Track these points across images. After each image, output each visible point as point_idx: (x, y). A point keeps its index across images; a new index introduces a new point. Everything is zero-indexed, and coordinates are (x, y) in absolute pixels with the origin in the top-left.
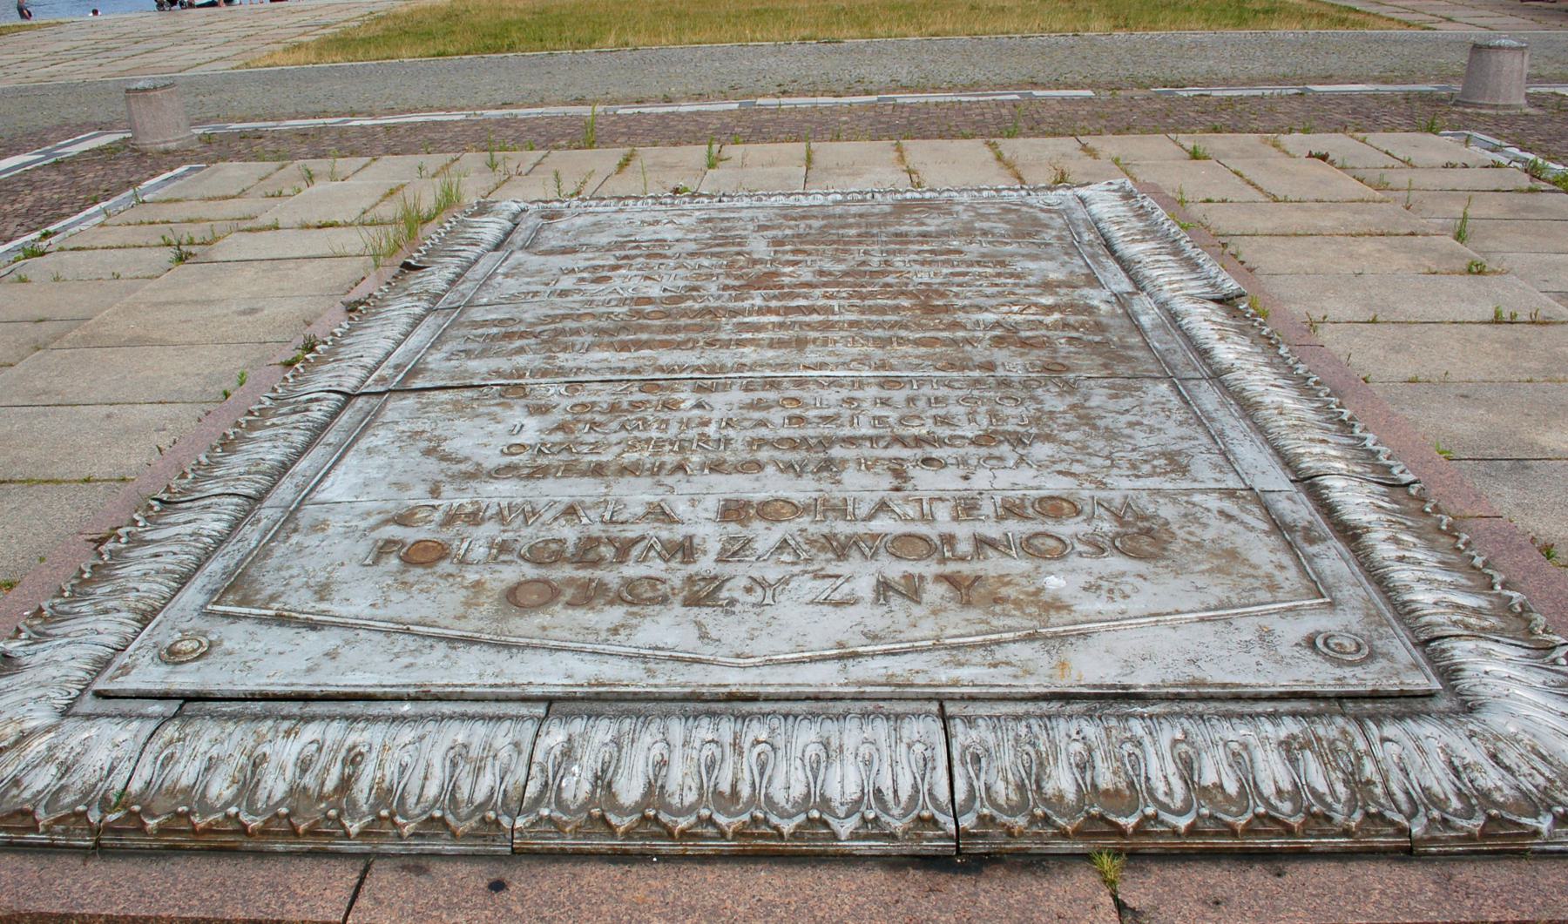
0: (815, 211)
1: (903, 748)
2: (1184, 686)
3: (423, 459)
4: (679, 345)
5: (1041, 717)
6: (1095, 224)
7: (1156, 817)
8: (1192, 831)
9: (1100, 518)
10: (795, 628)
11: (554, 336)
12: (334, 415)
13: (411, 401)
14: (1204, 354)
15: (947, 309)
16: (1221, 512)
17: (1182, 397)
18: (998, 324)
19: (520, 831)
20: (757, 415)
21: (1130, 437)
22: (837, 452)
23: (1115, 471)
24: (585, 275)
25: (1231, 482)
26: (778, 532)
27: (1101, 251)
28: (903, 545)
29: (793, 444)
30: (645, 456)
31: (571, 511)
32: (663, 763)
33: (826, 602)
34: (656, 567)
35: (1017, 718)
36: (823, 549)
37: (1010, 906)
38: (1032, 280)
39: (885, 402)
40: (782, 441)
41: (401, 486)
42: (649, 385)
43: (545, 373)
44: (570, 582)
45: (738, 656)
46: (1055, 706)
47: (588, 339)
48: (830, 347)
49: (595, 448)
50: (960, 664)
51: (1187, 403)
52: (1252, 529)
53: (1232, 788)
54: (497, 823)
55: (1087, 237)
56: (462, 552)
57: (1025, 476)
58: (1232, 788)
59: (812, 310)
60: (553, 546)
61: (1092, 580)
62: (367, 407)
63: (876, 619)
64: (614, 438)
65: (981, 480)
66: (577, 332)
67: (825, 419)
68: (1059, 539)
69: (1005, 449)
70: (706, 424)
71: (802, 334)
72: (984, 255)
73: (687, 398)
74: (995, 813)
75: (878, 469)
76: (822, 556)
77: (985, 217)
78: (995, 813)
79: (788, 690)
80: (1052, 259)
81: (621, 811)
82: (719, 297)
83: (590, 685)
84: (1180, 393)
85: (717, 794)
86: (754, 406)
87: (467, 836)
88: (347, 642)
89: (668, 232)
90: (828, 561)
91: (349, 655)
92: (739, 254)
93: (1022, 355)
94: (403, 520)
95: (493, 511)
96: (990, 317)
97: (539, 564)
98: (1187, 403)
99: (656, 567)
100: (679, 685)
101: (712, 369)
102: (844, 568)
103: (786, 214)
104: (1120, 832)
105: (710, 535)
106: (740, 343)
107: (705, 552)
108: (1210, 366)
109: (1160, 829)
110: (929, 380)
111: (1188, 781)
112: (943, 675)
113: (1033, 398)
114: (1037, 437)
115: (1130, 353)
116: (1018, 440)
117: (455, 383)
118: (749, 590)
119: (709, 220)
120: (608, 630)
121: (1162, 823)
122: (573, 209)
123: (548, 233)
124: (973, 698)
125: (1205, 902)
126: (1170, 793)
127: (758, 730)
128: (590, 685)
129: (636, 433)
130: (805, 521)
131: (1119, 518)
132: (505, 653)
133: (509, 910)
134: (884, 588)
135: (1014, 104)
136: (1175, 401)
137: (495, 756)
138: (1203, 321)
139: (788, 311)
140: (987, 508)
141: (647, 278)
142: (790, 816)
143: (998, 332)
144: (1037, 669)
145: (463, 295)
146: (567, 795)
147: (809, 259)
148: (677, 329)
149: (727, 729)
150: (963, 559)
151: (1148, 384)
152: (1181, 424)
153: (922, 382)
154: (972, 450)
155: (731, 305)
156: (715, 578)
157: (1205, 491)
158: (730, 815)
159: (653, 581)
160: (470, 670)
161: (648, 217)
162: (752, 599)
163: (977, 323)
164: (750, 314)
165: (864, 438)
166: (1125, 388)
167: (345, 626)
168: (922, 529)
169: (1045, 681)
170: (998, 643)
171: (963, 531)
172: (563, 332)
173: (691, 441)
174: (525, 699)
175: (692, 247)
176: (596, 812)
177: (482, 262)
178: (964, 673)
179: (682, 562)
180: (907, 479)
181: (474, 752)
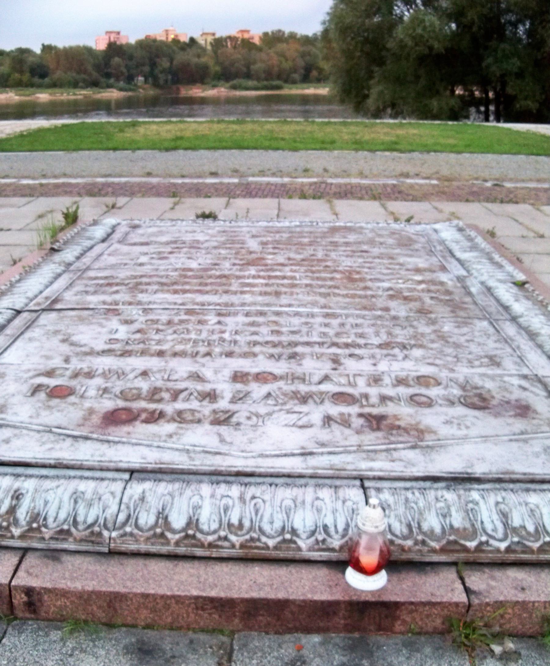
0: (284, 229)
1: (340, 503)
2: (502, 473)
3: (61, 344)
4: (207, 292)
5: (420, 489)
6: (442, 242)
7: (487, 542)
8: (508, 550)
9: (452, 387)
10: (276, 437)
11: (136, 286)
12: (10, 321)
13: (53, 315)
14: (506, 308)
15: (362, 280)
16: (521, 387)
17: (496, 329)
18: (390, 289)
19: (114, 539)
20: (253, 329)
21: (467, 347)
22: (299, 349)
23: (459, 364)
24: (154, 256)
25: (525, 371)
26: (266, 388)
27: (447, 254)
28: (340, 398)
29: (275, 345)
30: (188, 347)
31: (145, 374)
32: (197, 508)
33: (294, 425)
34: (194, 404)
35: (407, 489)
36: (292, 398)
37: (403, 589)
38: (410, 267)
39: (326, 325)
40: (267, 343)
41: (48, 358)
42: (189, 312)
43: (130, 304)
44: (145, 410)
45: (242, 451)
46: (428, 484)
47: (155, 287)
48: (295, 296)
49: (159, 342)
50: (373, 460)
51: (498, 331)
52: (537, 395)
53: (531, 528)
54: (100, 534)
55: (439, 248)
56: (82, 392)
57: (409, 365)
58: (531, 528)
59: (284, 278)
60: (135, 391)
61: (448, 418)
62: (29, 317)
63: (324, 435)
64: (170, 338)
65: (383, 366)
66: (149, 284)
67: (293, 332)
68: (428, 397)
69: (396, 351)
70: (223, 332)
71: (278, 289)
72: (382, 254)
73: (212, 319)
74: (394, 538)
75: (324, 358)
76: (291, 402)
77: (380, 236)
78: (394, 538)
79: (272, 470)
80: (420, 257)
81: (174, 532)
82: (231, 269)
83: (156, 463)
84: (494, 327)
85: (230, 525)
86: (253, 324)
87: (81, 540)
88: (15, 435)
89: (201, 237)
90: (295, 405)
91: (16, 443)
92: (242, 248)
93: (404, 304)
94: (50, 374)
95: (100, 371)
96: (386, 285)
97: (126, 400)
98: (498, 331)
99: (194, 404)
100: (209, 466)
101: (226, 305)
102: (304, 408)
103: (268, 230)
104: (466, 550)
105: (226, 389)
106: (242, 293)
107: (223, 398)
108: (510, 314)
109: (489, 548)
110: (352, 315)
111: (506, 525)
112: (364, 465)
113: (412, 326)
114: (415, 345)
115: (466, 306)
116: (404, 347)
117: (79, 307)
118: (249, 418)
119: (224, 232)
120: (167, 435)
121: (491, 546)
122: (147, 223)
123: (132, 235)
124: (380, 479)
125: (516, 588)
126: (495, 530)
127: (252, 491)
128: (156, 463)
129: (183, 336)
130: (281, 384)
131: (463, 388)
132: (106, 445)
133: (107, 582)
134: (328, 420)
135: (394, 186)
136: (491, 330)
137: (100, 499)
138: (506, 293)
139: (270, 277)
140: (387, 380)
141: (189, 258)
142: (273, 537)
143: (391, 292)
144: (420, 464)
145: (85, 264)
146: (142, 522)
147: (282, 252)
148: (206, 285)
149: (235, 491)
150: (373, 406)
151: (476, 321)
152: (496, 342)
153: (347, 316)
154: (377, 351)
155: (238, 273)
156: (227, 412)
157: (511, 375)
158: (236, 535)
159: (193, 411)
160: (86, 452)
161: (189, 229)
162: (250, 423)
163: (379, 288)
164: (248, 278)
165: (316, 343)
166: (463, 322)
167: (15, 427)
168: (349, 390)
169: (422, 469)
170: (395, 449)
171: (374, 392)
172: (141, 284)
173: (214, 341)
174: (118, 470)
175: (215, 244)
176: (158, 530)
177: (95, 248)
178: (376, 465)
179: (210, 402)
180: (340, 364)
181: (88, 496)
